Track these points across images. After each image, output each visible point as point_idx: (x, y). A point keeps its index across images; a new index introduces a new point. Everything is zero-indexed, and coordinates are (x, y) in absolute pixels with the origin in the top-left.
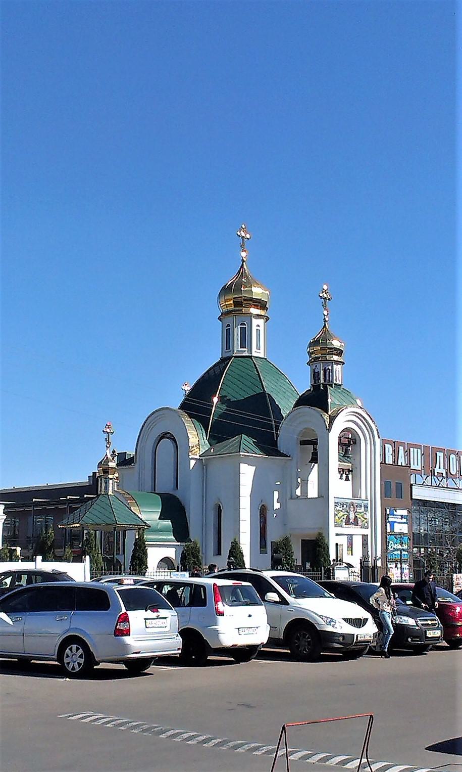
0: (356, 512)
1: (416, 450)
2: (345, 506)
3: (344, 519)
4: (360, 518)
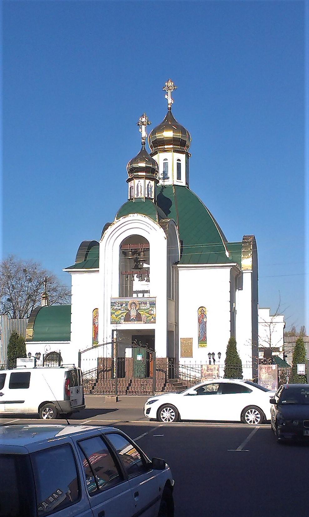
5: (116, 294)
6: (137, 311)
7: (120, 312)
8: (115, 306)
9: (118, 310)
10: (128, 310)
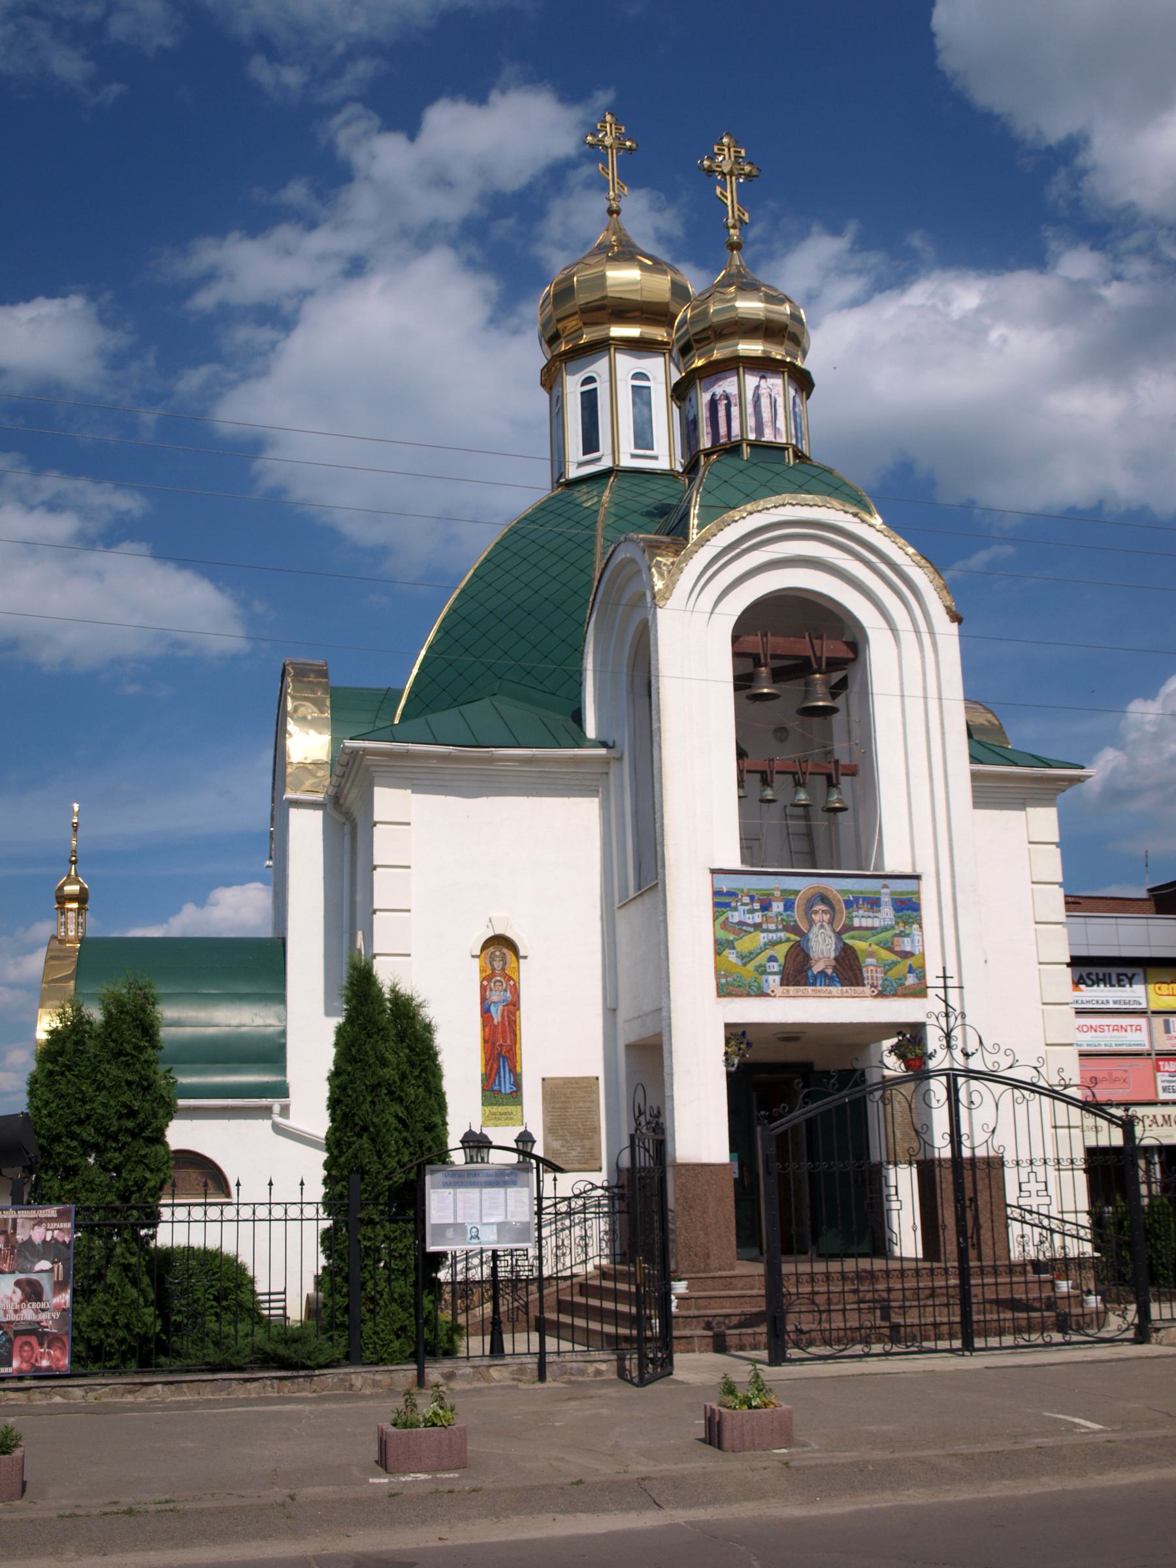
0: (848, 928)
1: (768, 436)
2: (778, 907)
3: (772, 959)
4: (871, 954)
5: (732, 859)
6: (839, 935)
7: (762, 938)
8: (736, 909)
9: (751, 929)
10: (795, 930)
